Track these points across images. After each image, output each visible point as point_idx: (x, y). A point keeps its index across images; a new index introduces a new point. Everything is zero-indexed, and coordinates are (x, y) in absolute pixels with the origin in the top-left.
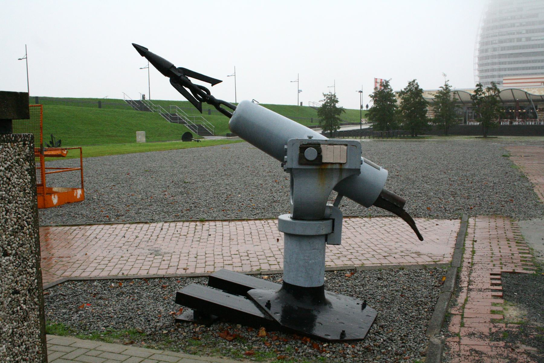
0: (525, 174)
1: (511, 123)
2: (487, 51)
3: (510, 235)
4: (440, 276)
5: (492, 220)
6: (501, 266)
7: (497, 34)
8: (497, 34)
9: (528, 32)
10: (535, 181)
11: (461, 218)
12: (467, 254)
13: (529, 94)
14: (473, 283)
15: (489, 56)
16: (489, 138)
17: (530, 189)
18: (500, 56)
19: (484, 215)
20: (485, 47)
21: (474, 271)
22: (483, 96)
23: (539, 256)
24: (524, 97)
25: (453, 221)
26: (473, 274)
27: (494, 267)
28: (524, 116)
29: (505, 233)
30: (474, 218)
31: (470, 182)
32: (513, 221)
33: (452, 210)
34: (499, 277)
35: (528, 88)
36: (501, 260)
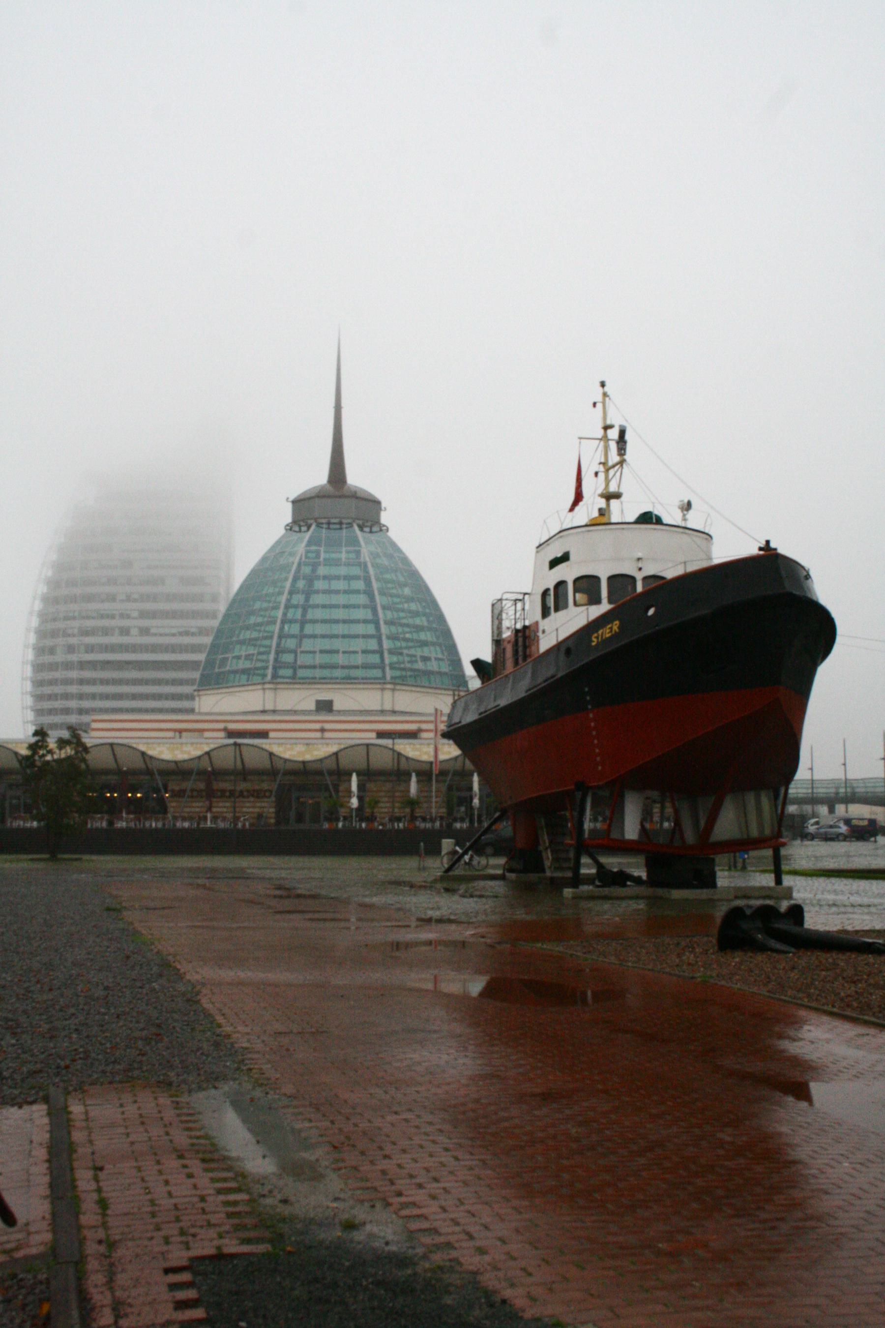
0: (170, 958)
1: (111, 823)
2: (52, 651)
3: (181, 1139)
4: (30, 1298)
5: (127, 1098)
6: (184, 1239)
7: (76, 614)
8: (76, 614)
9: (143, 615)
10: (197, 977)
11: (46, 1100)
12: (89, 1217)
13: (151, 757)
14: (129, 1310)
15: (57, 663)
16: (65, 860)
17: (192, 999)
18: (83, 665)
19: (102, 1084)
20: (49, 642)
21: (120, 1269)
22: (49, 758)
23: (264, 1196)
24: (139, 764)
25: (26, 1108)
26: (122, 1279)
27: (170, 1247)
28: (137, 808)
29: (167, 1134)
30: (80, 1096)
31: (46, 988)
32: (177, 1096)
33: (18, 1077)
34: (186, 1277)
35: (148, 743)
36: (178, 1220)
